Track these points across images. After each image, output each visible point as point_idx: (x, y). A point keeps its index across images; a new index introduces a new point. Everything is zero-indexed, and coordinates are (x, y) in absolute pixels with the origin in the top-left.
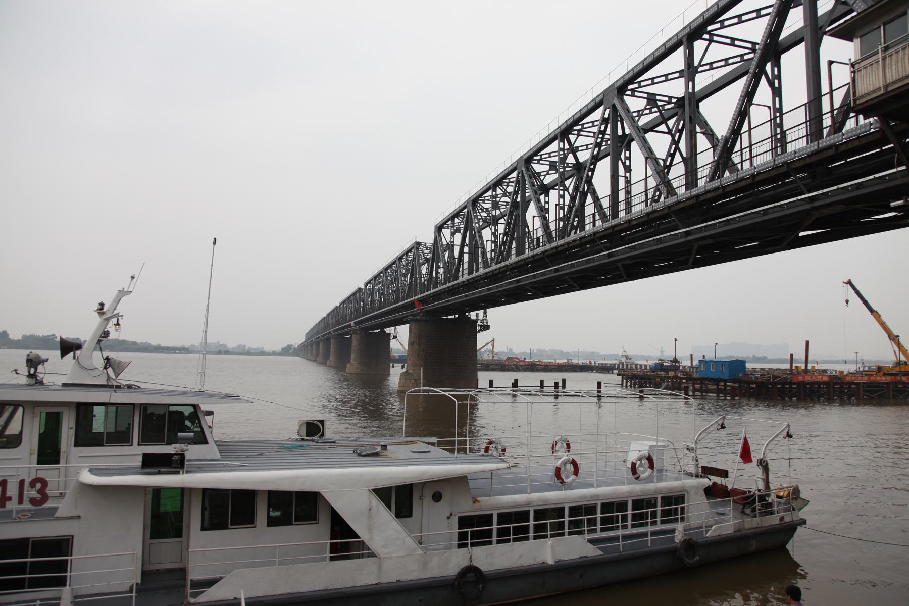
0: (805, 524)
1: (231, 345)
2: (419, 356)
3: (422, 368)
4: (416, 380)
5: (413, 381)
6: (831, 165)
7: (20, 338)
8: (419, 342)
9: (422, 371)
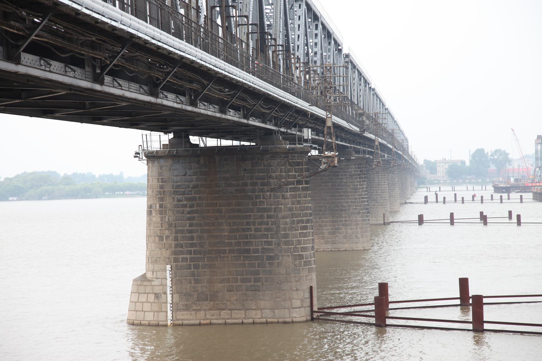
2: (161, 238)
3: (168, 267)
4: (157, 296)
5: (152, 298)
8: (161, 206)
9: (168, 273)
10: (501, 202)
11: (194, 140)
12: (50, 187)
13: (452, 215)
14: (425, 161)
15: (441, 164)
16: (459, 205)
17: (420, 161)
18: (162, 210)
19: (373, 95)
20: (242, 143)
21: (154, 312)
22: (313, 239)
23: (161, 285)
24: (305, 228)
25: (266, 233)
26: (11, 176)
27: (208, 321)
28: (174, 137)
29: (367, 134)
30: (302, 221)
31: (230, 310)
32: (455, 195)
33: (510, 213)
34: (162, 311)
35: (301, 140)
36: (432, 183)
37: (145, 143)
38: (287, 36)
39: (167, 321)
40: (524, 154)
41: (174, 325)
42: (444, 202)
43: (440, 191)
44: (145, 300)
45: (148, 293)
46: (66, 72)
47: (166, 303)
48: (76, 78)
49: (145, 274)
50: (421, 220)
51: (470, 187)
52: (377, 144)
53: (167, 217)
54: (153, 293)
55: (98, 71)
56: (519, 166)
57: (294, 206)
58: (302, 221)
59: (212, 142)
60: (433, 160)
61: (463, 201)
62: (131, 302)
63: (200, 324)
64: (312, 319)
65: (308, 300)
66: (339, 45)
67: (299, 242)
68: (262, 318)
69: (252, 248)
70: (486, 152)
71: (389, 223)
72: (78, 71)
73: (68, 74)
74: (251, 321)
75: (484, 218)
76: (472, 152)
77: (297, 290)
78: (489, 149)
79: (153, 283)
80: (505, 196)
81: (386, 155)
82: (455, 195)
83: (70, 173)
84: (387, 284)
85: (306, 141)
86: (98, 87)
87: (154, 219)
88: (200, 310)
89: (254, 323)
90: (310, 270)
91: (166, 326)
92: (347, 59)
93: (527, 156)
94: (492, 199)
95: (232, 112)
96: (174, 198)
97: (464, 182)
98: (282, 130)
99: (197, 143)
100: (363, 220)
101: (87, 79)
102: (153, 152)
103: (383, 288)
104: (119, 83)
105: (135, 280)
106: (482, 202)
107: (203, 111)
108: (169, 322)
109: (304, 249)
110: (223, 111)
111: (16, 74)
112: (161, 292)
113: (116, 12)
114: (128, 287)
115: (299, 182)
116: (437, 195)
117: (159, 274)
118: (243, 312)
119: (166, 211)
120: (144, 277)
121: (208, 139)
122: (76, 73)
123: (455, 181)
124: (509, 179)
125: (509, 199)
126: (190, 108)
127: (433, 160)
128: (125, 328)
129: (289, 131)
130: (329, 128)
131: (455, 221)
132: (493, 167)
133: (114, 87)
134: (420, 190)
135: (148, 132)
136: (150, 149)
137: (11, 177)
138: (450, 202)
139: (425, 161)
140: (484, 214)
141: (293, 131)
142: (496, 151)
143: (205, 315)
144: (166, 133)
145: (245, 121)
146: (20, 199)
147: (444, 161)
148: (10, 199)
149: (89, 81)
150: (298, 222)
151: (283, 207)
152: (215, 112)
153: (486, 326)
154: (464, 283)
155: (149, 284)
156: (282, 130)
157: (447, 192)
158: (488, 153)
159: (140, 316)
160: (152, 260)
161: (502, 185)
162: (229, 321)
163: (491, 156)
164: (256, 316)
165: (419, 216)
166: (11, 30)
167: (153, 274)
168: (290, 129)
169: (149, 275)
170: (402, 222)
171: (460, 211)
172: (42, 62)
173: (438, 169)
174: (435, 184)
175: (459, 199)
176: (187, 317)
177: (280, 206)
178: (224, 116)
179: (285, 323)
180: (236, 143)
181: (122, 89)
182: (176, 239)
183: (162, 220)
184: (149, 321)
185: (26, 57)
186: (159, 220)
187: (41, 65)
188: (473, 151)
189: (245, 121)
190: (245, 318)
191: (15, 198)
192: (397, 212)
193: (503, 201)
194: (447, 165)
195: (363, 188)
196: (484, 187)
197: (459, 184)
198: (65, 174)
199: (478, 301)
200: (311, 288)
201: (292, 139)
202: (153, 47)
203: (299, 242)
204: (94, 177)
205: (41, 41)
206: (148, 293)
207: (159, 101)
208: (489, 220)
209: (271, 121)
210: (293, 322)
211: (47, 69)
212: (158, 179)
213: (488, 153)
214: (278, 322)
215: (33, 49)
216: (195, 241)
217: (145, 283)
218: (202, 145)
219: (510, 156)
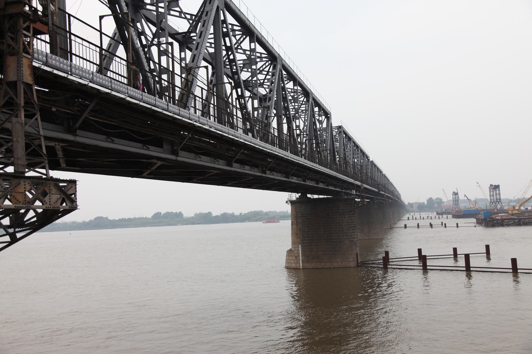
0: (49, 167)
1: (216, 213)
2: (297, 235)
3: (300, 246)
4: (296, 257)
5: (294, 258)
6: (214, 142)
7: (219, 215)
8: (296, 222)
9: (300, 248)
10: (439, 219)
11: (309, 196)
12: (260, 217)
13: (418, 224)
14: (408, 203)
15: (415, 204)
16: (422, 220)
17: (406, 203)
18: (297, 224)
19: (384, 177)
20: (328, 196)
21: (295, 263)
22: (357, 234)
23: (298, 253)
24: (354, 229)
25: (338, 232)
26: (246, 213)
28: (301, 195)
29: (381, 192)
30: (352, 227)
31: (325, 262)
32: (420, 216)
33: (442, 223)
34: (298, 263)
35: (351, 194)
36: (411, 212)
37: (290, 198)
38: (345, 154)
39: (300, 267)
40: (449, 200)
41: (303, 269)
42: (416, 219)
43: (414, 215)
44: (291, 259)
46: (251, 170)
47: (300, 260)
48: (201, 161)
49: (291, 249)
50: (406, 226)
51: (427, 213)
52: (385, 196)
53: (299, 226)
55: (264, 169)
56: (447, 204)
57: (349, 221)
58: (352, 227)
59: (316, 196)
60: (411, 202)
61: (423, 219)
62: (286, 259)
63: (313, 268)
64: (358, 266)
65: (356, 258)
66: (368, 158)
67: (352, 235)
69: (333, 238)
70: (433, 199)
71: (393, 228)
72: (256, 169)
73: (252, 170)
74: (333, 267)
75: (431, 225)
76: (427, 199)
77: (351, 254)
78: (434, 198)
79: (294, 252)
80: (441, 216)
81: (390, 201)
82: (420, 216)
83: (268, 211)
84: (388, 252)
85: (353, 195)
86: (264, 175)
87: (294, 227)
88: (313, 263)
89: (334, 268)
90: (357, 246)
91: (300, 269)
92: (372, 163)
93: (450, 200)
94: (435, 218)
95: (321, 184)
96: (301, 219)
97: (425, 211)
98: (344, 191)
99: (310, 197)
100: (381, 227)
101: (164, 152)
102: (293, 201)
103: (387, 253)
104: (273, 174)
105: (287, 251)
106: (431, 219)
107: (308, 184)
108: (301, 267)
109: (354, 238)
110: (230, 165)
111: (231, 171)
112: (298, 255)
113: (258, 142)
114: (285, 254)
115: (351, 211)
116: (413, 216)
118: (330, 263)
119: (298, 224)
120: (291, 250)
121: (314, 195)
122: (219, 162)
123: (421, 211)
124: (443, 209)
125: (442, 217)
126: (303, 183)
127: (411, 203)
128: (285, 270)
129: (346, 191)
130: (362, 189)
131: (420, 226)
132: (436, 205)
133: (271, 175)
134: (407, 215)
135: (291, 193)
136: (292, 200)
137: (246, 213)
138: (418, 219)
139: (408, 203)
140: (431, 223)
141: (348, 191)
142: (437, 198)
143: (315, 264)
144: (297, 193)
145: (327, 187)
146: (249, 221)
147: (416, 203)
148: (246, 221)
149: (168, 154)
150: (351, 227)
151: (345, 221)
152: (314, 184)
153: (428, 268)
154: (420, 251)
155: (292, 252)
156: (344, 191)
157: (417, 215)
158: (434, 199)
159: (290, 265)
160: (293, 243)
161: (439, 212)
162: (325, 267)
163: (435, 200)
164: (335, 265)
165: (405, 225)
166: (229, 155)
168: (347, 190)
169: (293, 249)
170: (396, 227)
171: (421, 223)
172: (242, 166)
173: (414, 206)
174: (413, 212)
175: (422, 218)
176: (308, 265)
177: (343, 221)
178: (318, 186)
179: (347, 267)
180: (325, 197)
181: (149, 150)
182: (303, 235)
183: (297, 227)
184: (293, 267)
185: (235, 165)
186: (296, 227)
187: (241, 168)
188: (428, 199)
189: (327, 187)
190: (331, 266)
191: (248, 221)
192: (396, 223)
193: (440, 218)
194: (418, 204)
195: (380, 214)
196: (432, 213)
197: (422, 212)
198: (266, 212)
200: (357, 253)
201: (348, 194)
202: (285, 159)
203: (352, 235)
204: (277, 212)
205: (241, 158)
207: (290, 180)
208: (433, 226)
209: (339, 187)
210: (350, 267)
211: (244, 169)
212: (295, 211)
213: (434, 199)
214: (344, 267)
215: (238, 161)
216: (310, 236)
217: (291, 252)
218: (312, 198)
219: (443, 201)
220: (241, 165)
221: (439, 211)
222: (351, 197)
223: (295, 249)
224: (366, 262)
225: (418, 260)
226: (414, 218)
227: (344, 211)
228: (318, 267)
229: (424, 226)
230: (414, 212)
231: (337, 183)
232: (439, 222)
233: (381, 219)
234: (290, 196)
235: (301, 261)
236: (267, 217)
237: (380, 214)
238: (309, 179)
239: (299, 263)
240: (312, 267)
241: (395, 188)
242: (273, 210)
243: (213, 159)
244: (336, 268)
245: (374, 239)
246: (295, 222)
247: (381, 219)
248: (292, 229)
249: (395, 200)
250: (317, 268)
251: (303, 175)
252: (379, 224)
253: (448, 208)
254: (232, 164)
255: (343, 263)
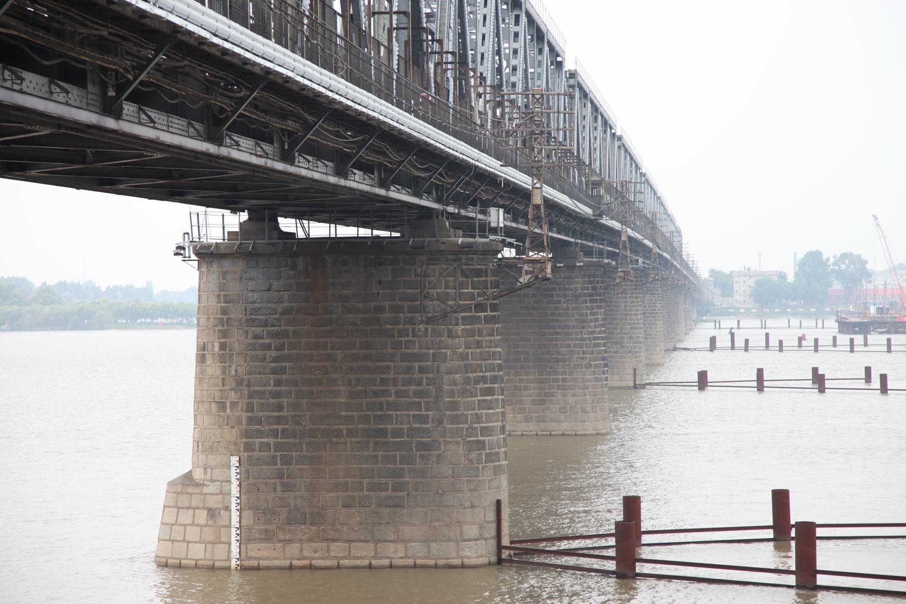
2: (222, 406)
3: (234, 460)
4: (212, 513)
5: (202, 517)
8: (223, 346)
9: (233, 471)
10: (852, 351)
11: (287, 224)
14: (712, 271)
16: (774, 354)
17: (703, 272)
18: (225, 354)
19: (619, 147)
20: (376, 232)
21: (206, 543)
23: (221, 493)
24: (489, 392)
27: (306, 562)
28: (250, 219)
29: (606, 221)
30: (484, 380)
32: (767, 335)
33: (868, 370)
34: (220, 543)
35: (485, 229)
36: (725, 313)
37: (195, 229)
38: (462, 35)
41: (243, 569)
42: (746, 348)
43: (738, 328)
45: (195, 509)
46: (51, 93)
47: (230, 526)
49: (191, 472)
50: (703, 381)
51: (795, 322)
53: (234, 367)
54: (204, 508)
55: (111, 93)
56: (885, 285)
57: (470, 351)
58: (484, 380)
59: (319, 230)
62: (163, 523)
63: (291, 567)
64: (500, 561)
65: (493, 526)
66: (558, 55)
68: (406, 557)
70: (825, 257)
73: (55, 97)
74: (386, 562)
75: (819, 380)
77: (473, 506)
78: (830, 253)
80: (859, 339)
81: (641, 260)
82: (767, 335)
83: (52, 282)
85: (494, 231)
86: (110, 123)
87: (210, 371)
88: (291, 541)
90: (497, 471)
92: (572, 82)
94: (835, 345)
96: (247, 332)
97: (784, 313)
98: (451, 209)
100: (596, 380)
102: (210, 246)
103: (632, 505)
105: (171, 484)
106: (816, 350)
107: (304, 172)
108: (234, 563)
109: (486, 431)
112: (220, 506)
114: (159, 495)
115: (480, 307)
117: (217, 474)
118: (371, 546)
120: (188, 478)
121: (313, 224)
122: (70, 95)
124: (866, 308)
125: (866, 345)
126: (280, 166)
127: (727, 271)
129: (463, 212)
130: (537, 207)
131: (766, 384)
132: (837, 286)
133: (140, 123)
135: (203, 208)
136: (204, 240)
138: (757, 349)
139: (712, 271)
142: (844, 256)
143: (301, 550)
144: (234, 211)
145: (382, 192)
147: (748, 273)
152: (327, 174)
153: (821, 580)
154: (781, 499)
156: (451, 209)
158: (828, 259)
159: (180, 551)
160: (203, 446)
161: (853, 320)
163: (835, 264)
164: (396, 553)
165: (699, 373)
167: (205, 473)
169: (198, 475)
172: (7, 73)
174: (729, 314)
175: (774, 343)
177: (444, 351)
178: (343, 182)
179: (451, 567)
180: (364, 232)
182: (250, 408)
183: (223, 373)
184: (196, 561)
187: (5, 80)
188: (801, 255)
189: (382, 192)
195: (597, 320)
199: (807, 532)
200: (499, 503)
201: (468, 227)
202: (214, 51)
203: (478, 418)
206: (195, 509)
207: (224, 151)
208: (828, 384)
209: (429, 193)
210: (463, 566)
211: (16, 87)
212: (219, 296)
213: (828, 259)
214: (436, 567)
216: (285, 413)
217: (191, 490)
218: (301, 235)
220: (4, 68)
221: (852, 313)
222: (487, 240)
223: (208, 477)
224: (542, 545)
225: (772, 544)
226: (737, 344)
227: (450, 303)
228: (315, 562)
229: (786, 385)
230: (735, 312)
231: (426, 170)
232: (854, 366)
233: (599, 345)
234: (195, 222)
235: (234, 532)
236: (47, 309)
237: (597, 320)
238: (142, 98)
239: (223, 540)
240: (287, 563)
241: (662, 204)
242: (76, 275)
243: (185, 124)
244: (398, 567)
245: (563, 435)
246: (217, 348)
247: (599, 345)
248: (200, 379)
249: (660, 256)
250: (311, 567)
251: (282, 130)
252: (589, 366)
253: (891, 304)
254: (121, 103)
255: (433, 545)
